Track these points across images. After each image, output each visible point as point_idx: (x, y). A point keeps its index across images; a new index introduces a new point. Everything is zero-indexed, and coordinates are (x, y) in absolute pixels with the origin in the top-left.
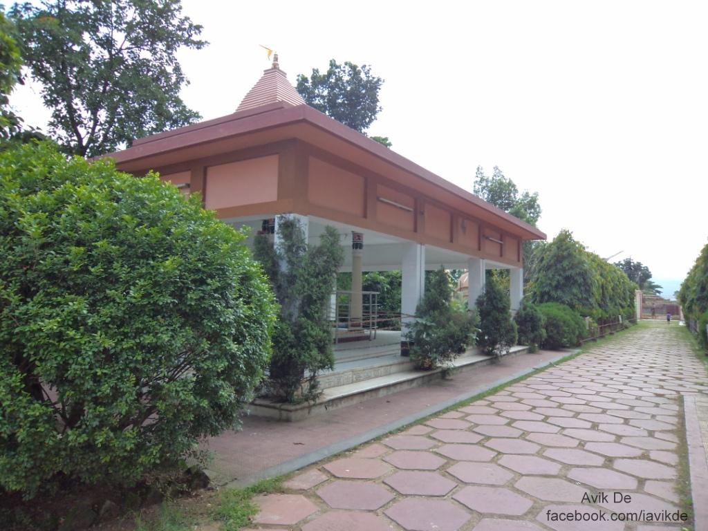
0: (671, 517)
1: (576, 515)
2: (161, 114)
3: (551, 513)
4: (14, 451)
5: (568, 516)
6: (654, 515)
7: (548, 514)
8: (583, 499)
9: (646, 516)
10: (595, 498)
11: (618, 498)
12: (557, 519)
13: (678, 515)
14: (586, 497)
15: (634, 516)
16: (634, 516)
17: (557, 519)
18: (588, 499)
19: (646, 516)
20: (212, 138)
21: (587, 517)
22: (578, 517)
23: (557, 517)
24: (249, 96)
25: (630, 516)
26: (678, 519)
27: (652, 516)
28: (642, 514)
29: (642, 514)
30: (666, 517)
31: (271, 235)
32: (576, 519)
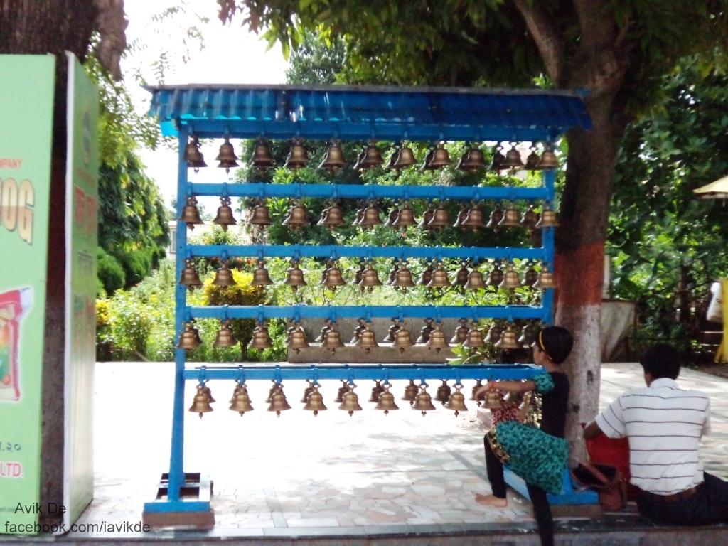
3: (10, 524)
5: (26, 528)
6: (133, 530)
9: (107, 528)
13: (140, 526)
14: (19, 508)
16: (95, 527)
18: (22, 509)
25: (91, 527)
26: (140, 531)
27: (113, 528)
28: (103, 526)
29: (103, 526)
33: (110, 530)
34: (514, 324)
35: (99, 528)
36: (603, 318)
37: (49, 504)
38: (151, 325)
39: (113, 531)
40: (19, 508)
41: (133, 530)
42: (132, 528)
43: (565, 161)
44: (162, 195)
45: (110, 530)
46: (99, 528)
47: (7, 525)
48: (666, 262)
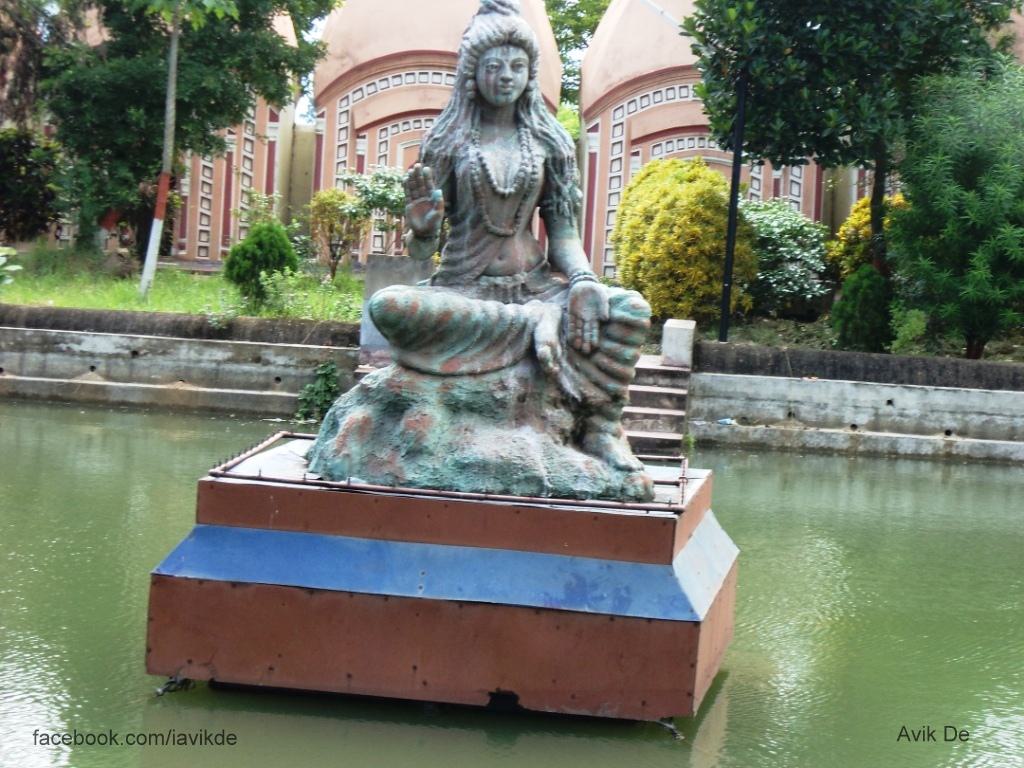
0: (212, 738)
1: (75, 737)
2: (342, 218)
3: (39, 733)
4: (993, 421)
5: (63, 739)
6: (188, 739)
8: (900, 735)
10: (208, 734)
11: (951, 735)
12: (48, 743)
13: (223, 736)
14: (904, 733)
15: (160, 738)
16: (160, 738)
17: (185, 743)
20: (329, 588)
21: (91, 739)
24: (284, 443)
25: (153, 738)
28: (171, 738)
29: (171, 736)
30: (206, 739)
32: (75, 743)
33: (43, 742)
34: (258, 299)
35: (165, 739)
36: (478, 367)
38: (260, 245)
39: (185, 743)
40: (904, 733)
41: (188, 739)
42: (212, 738)
43: (974, 268)
44: (689, 27)
45: (43, 742)
46: (165, 739)
47: (35, 735)
48: (624, 303)
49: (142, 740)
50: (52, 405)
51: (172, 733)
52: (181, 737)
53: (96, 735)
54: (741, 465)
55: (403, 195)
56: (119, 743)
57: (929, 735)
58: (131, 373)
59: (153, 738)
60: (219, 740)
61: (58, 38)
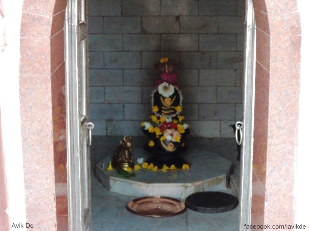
5: (253, 227)
7: (245, 226)
8: (13, 226)
9: (288, 227)
11: (28, 225)
14: (14, 225)
18: (15, 226)
19: (288, 227)
22: (277, 227)
23: (249, 227)
25: (281, 227)
27: (290, 227)
28: (286, 226)
29: (286, 226)
31: (139, 158)
37: (26, 224)
39: (290, 228)
40: (14, 225)
42: (298, 227)
47: (245, 226)
49: (277, 227)
50: (81, 62)
51: (286, 225)
52: (255, 228)
53: (260, 228)
54: (55, 194)
55: (149, 144)
56: (270, 228)
57: (21, 226)
58: (123, 49)
59: (281, 227)
60: (301, 227)
61: (299, 60)
